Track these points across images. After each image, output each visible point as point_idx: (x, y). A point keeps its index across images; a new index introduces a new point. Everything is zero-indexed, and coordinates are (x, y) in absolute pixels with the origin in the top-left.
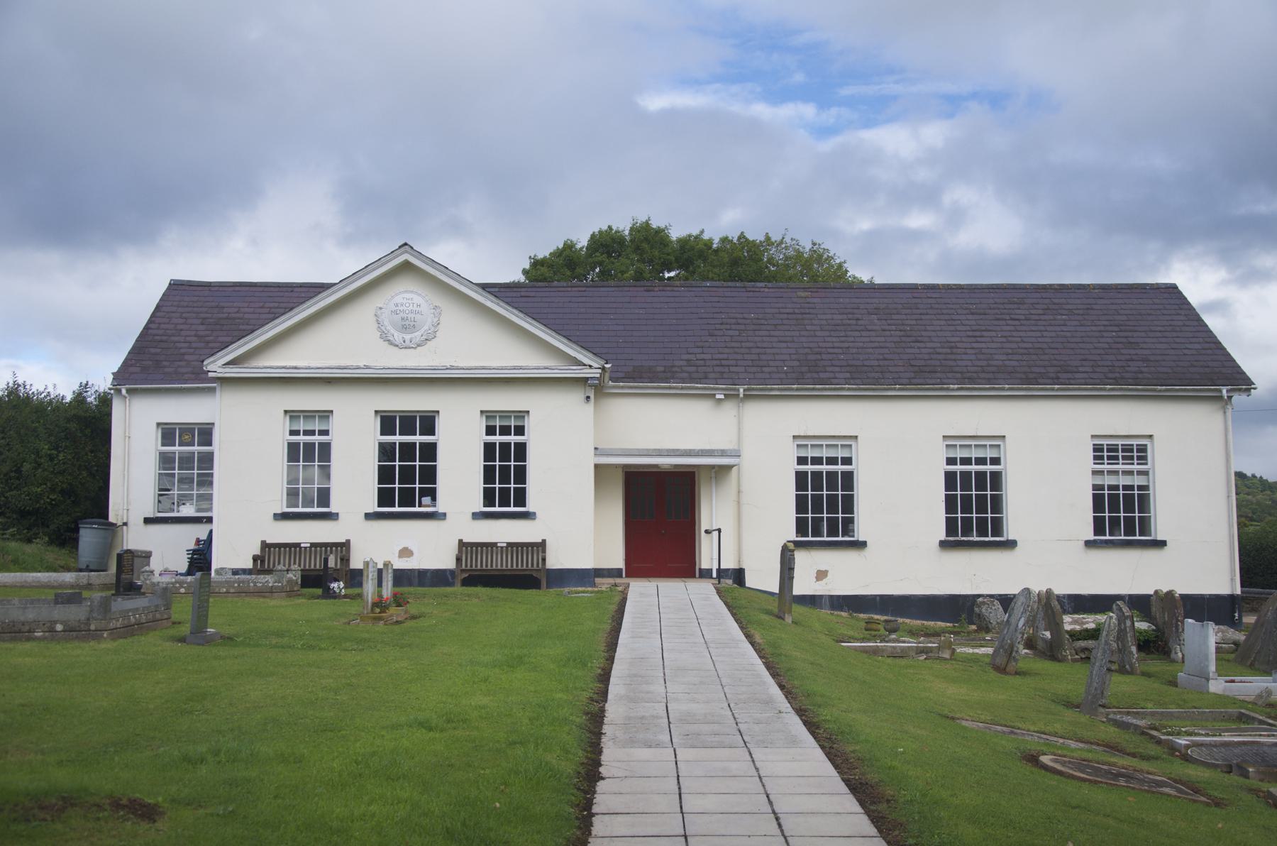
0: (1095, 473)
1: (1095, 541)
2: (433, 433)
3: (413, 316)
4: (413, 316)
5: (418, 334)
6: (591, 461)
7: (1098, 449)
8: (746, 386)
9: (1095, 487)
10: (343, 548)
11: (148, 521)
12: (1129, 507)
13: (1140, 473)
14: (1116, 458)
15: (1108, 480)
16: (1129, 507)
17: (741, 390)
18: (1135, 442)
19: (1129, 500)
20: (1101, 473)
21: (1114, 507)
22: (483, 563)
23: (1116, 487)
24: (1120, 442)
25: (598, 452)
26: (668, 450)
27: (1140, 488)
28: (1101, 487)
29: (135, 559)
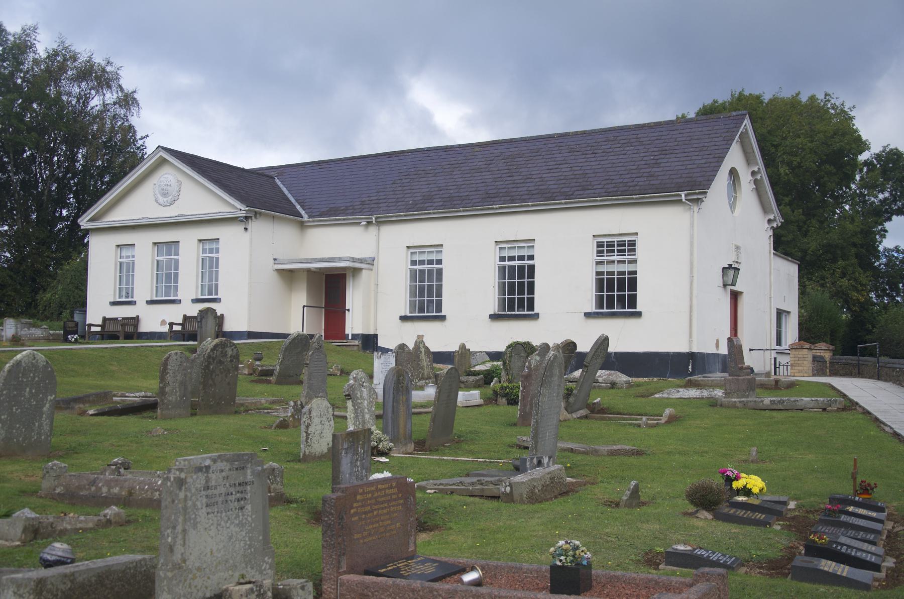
0: (599, 263)
1: (597, 313)
2: (178, 255)
3: (166, 187)
4: (166, 187)
5: (170, 197)
6: (271, 266)
7: (600, 245)
8: (686, 192)
9: (598, 273)
10: (136, 320)
11: (151, 302)
12: (621, 288)
13: (631, 262)
14: (613, 251)
15: (605, 268)
16: (621, 288)
17: (683, 196)
18: (626, 239)
19: (621, 282)
20: (601, 263)
21: (610, 288)
22: (110, 328)
23: (613, 273)
24: (616, 239)
25: (276, 262)
26: (312, 259)
27: (630, 273)
28: (601, 273)
29: (181, 322)
